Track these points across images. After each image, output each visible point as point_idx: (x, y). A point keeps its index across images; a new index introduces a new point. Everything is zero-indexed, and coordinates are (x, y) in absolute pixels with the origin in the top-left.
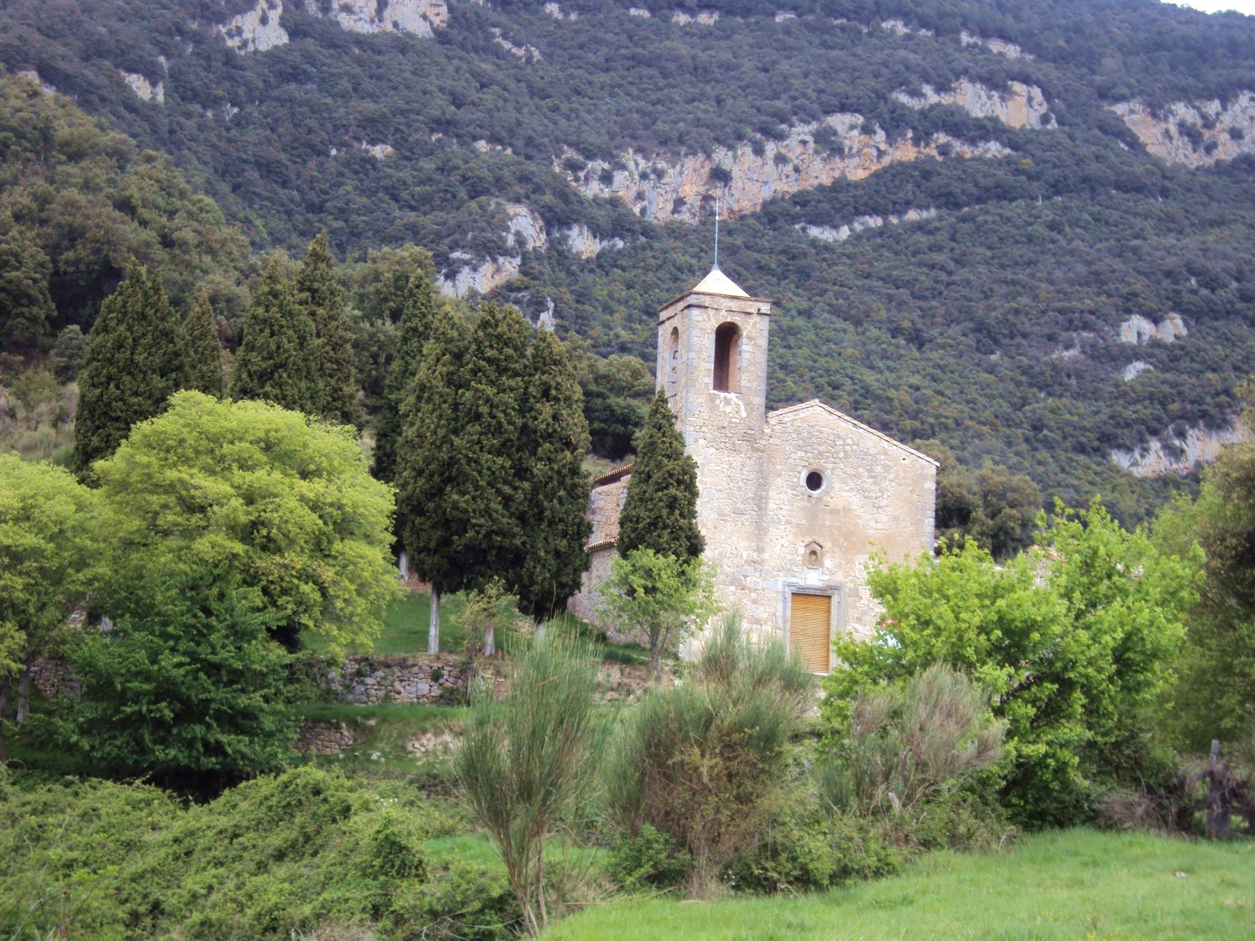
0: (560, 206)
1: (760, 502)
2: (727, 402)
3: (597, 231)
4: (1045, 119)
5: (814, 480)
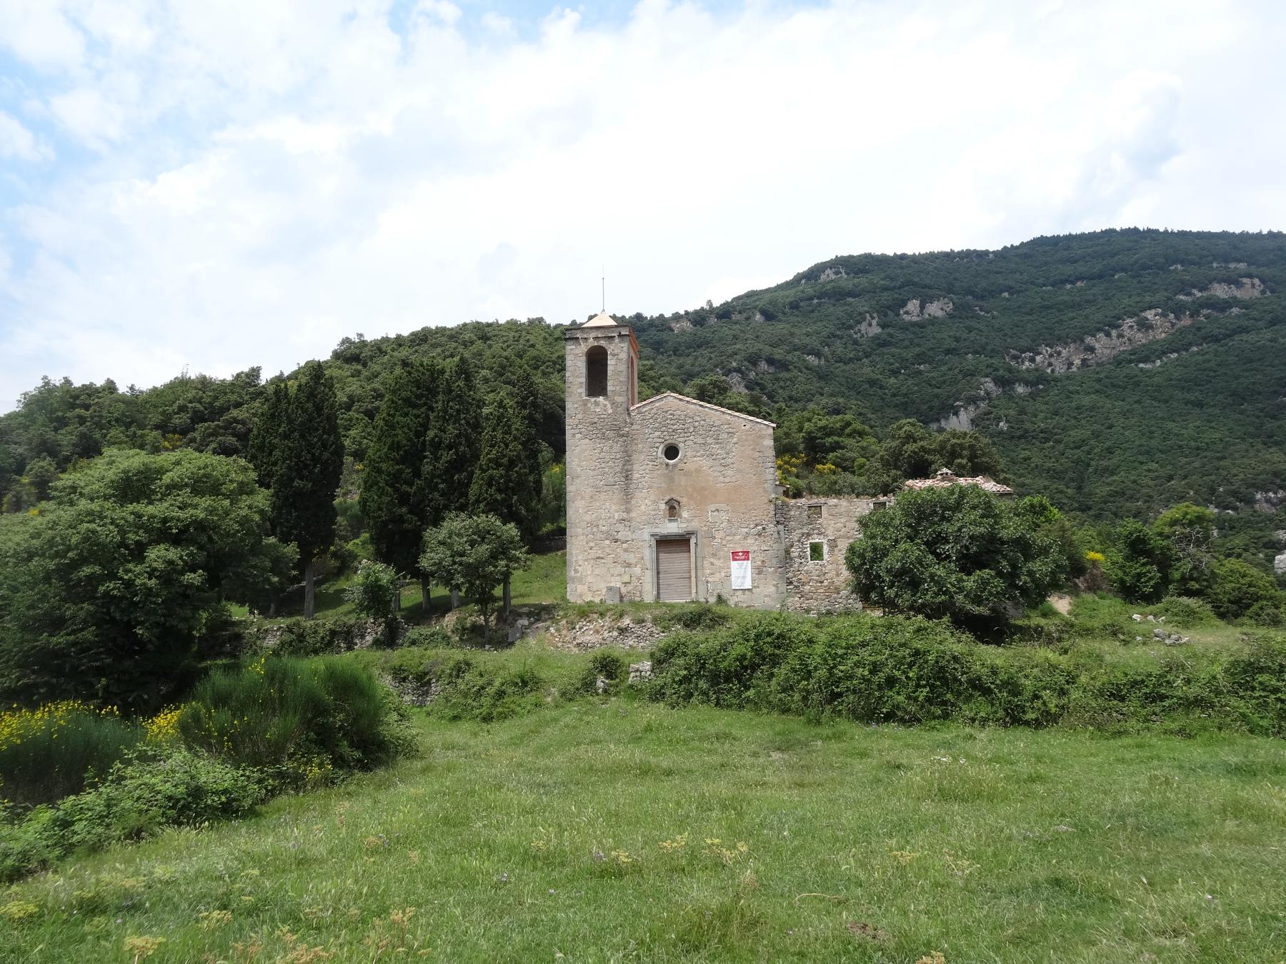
0: (1007, 375)
2: (597, 404)
3: (1027, 383)
4: (1263, 292)
5: (671, 452)
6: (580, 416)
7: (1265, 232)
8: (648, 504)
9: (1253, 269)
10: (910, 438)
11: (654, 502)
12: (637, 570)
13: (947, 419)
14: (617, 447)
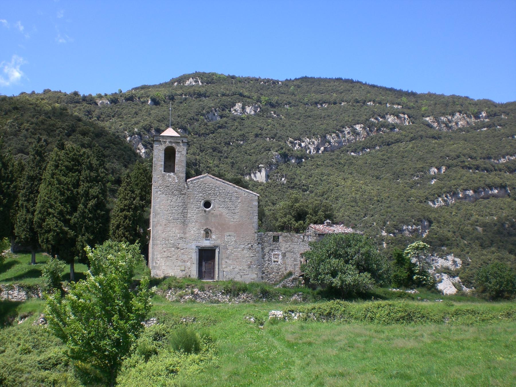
1: (184, 214)
5: (207, 204)
6: (160, 182)
7: (410, 91)
8: (195, 230)
9: (405, 110)
10: (296, 200)
11: (198, 229)
12: (189, 264)
13: (255, 174)
14: (179, 200)
